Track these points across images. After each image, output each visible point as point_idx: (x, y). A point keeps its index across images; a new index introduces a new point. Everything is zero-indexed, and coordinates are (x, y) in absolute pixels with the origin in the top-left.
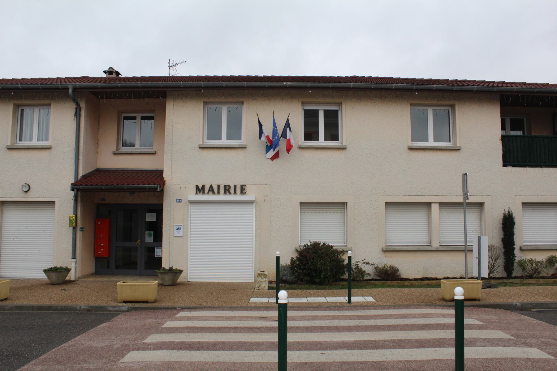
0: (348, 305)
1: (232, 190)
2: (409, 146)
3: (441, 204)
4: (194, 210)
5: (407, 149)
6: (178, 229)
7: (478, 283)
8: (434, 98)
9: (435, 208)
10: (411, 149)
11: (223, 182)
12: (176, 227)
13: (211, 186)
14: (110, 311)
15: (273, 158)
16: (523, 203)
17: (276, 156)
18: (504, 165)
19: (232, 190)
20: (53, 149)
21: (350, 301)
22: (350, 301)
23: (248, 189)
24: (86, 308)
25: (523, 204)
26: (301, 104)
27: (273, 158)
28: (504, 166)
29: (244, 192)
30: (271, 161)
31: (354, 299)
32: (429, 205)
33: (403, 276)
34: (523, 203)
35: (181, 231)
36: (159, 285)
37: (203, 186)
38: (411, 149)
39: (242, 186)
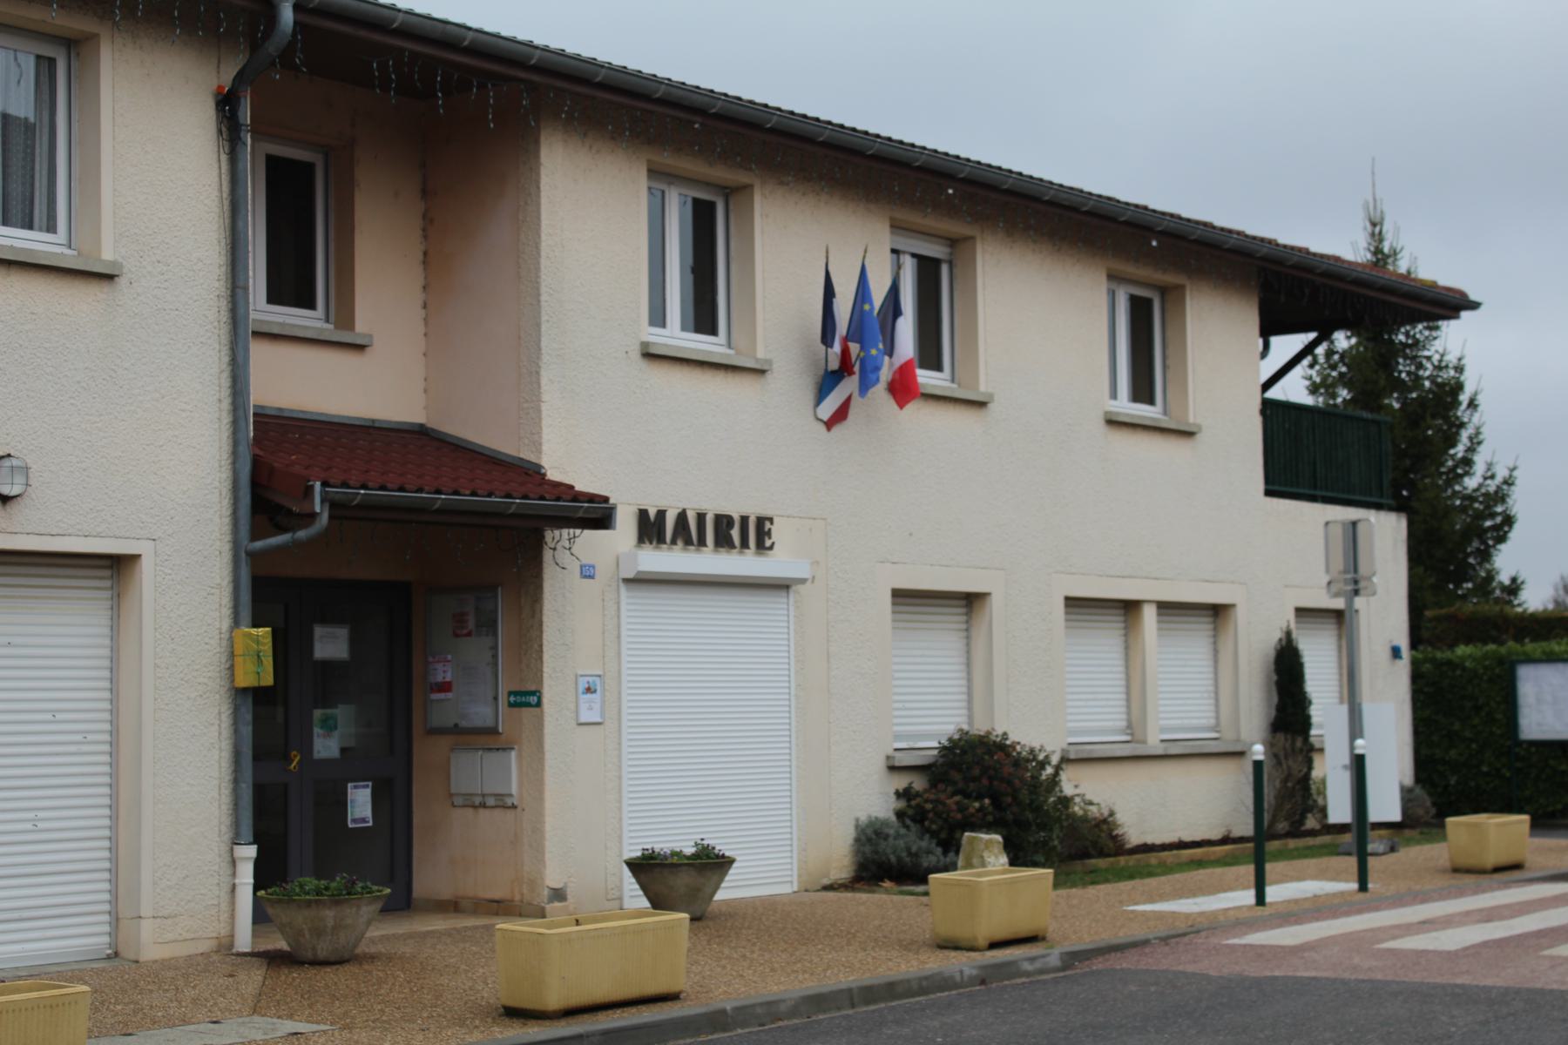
0: (1362, 895)
1: (735, 533)
2: (1106, 413)
3: (1165, 607)
4: (637, 609)
5: (1102, 422)
6: (589, 690)
7: (1520, 822)
8: (1156, 260)
9: (1149, 614)
10: (1113, 422)
11: (714, 505)
12: (582, 685)
13: (682, 518)
14: (1028, 974)
15: (830, 424)
16: (1067, 599)
17: (841, 415)
18: (1269, 493)
19: (735, 533)
20: (122, 282)
21: (1260, 899)
22: (1260, 899)
23: (778, 532)
24: (974, 972)
25: (901, 596)
26: (644, 173)
27: (830, 424)
28: (1269, 493)
29: (768, 543)
30: (823, 428)
31: (1273, 893)
32: (1130, 608)
33: (1134, 838)
34: (1067, 599)
35: (596, 697)
36: (692, 919)
37: (661, 514)
38: (1113, 422)
39: (761, 521)
